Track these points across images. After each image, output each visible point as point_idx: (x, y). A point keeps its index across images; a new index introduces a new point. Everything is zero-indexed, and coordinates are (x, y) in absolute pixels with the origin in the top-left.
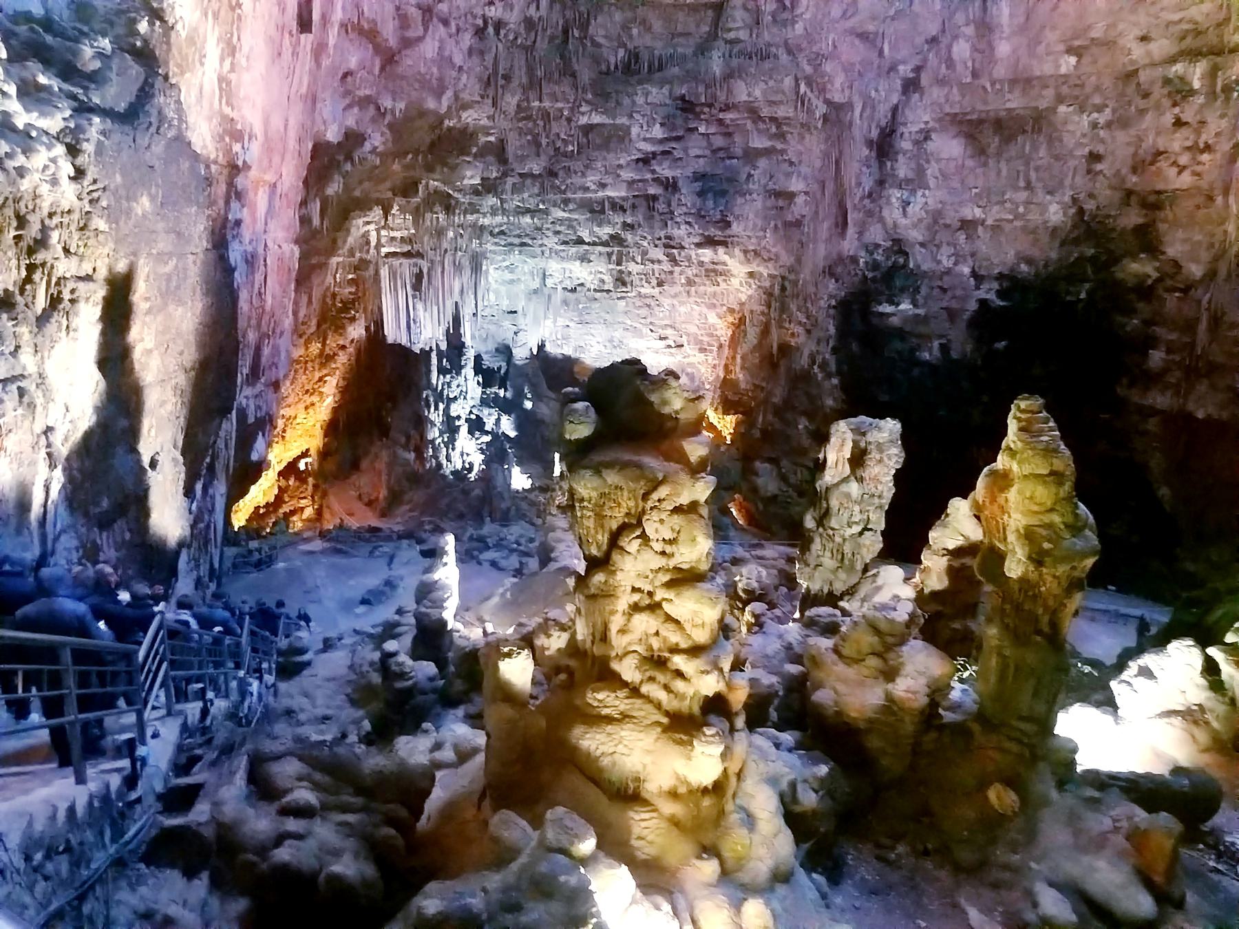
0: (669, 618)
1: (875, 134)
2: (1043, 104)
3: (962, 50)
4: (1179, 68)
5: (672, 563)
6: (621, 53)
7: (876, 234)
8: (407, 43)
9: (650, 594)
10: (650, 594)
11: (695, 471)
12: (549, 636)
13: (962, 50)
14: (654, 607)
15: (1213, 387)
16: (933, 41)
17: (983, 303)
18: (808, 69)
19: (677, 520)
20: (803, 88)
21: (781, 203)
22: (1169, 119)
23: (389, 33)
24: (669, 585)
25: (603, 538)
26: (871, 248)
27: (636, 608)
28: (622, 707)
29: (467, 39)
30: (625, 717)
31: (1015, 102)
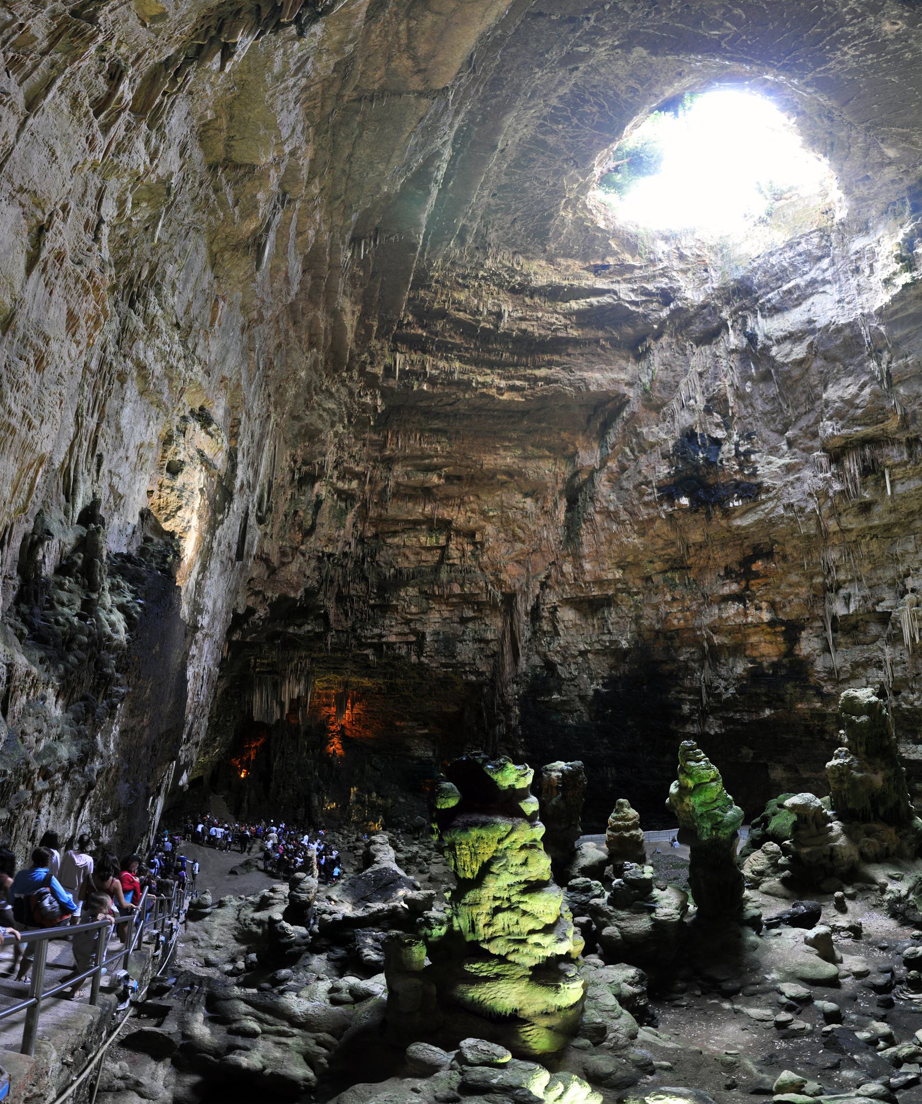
0: (525, 913)
1: (529, 608)
2: (611, 592)
3: (568, 568)
4: (669, 574)
5: (523, 879)
6: (392, 571)
7: (536, 660)
8: (283, 564)
9: (509, 899)
10: (509, 899)
11: (531, 820)
12: (431, 929)
13: (568, 568)
14: (511, 909)
15: (715, 718)
16: (554, 563)
17: (596, 691)
18: (492, 578)
19: (524, 854)
20: (490, 587)
21: (482, 645)
22: (668, 597)
23: (275, 559)
24: (524, 892)
25: (476, 867)
26: (534, 667)
27: (497, 910)
28: (495, 971)
29: (313, 563)
30: (498, 977)
31: (596, 592)
